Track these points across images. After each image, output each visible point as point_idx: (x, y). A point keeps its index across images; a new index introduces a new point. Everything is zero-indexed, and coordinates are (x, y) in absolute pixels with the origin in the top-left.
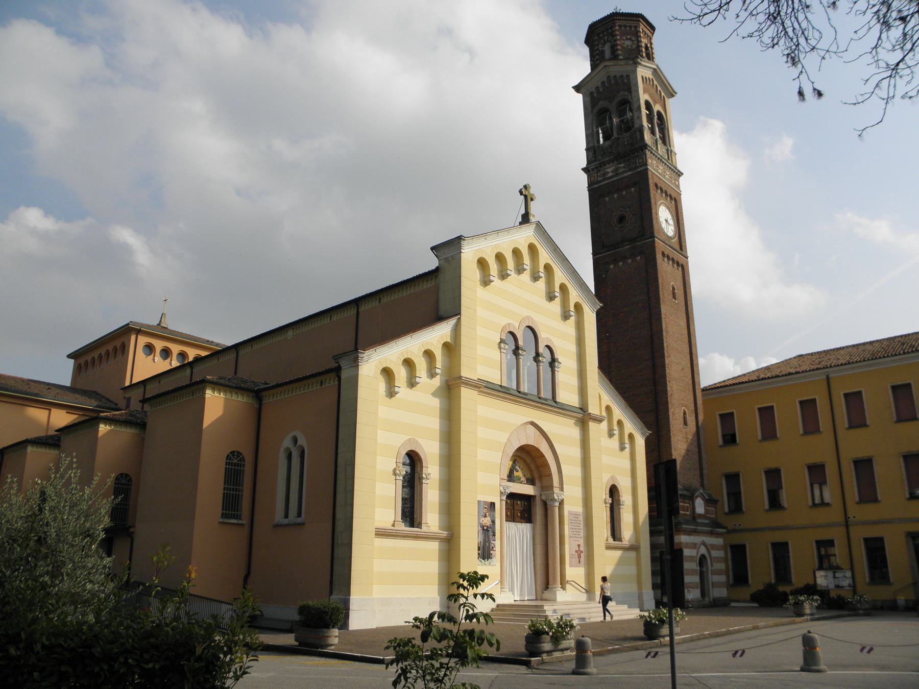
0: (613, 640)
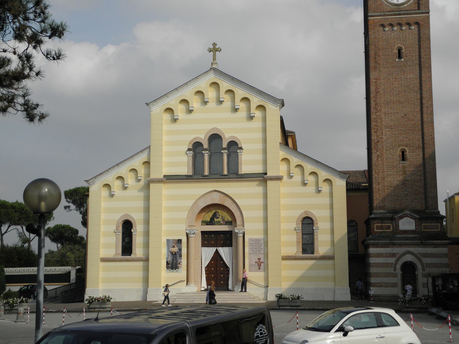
0: (308, 259)
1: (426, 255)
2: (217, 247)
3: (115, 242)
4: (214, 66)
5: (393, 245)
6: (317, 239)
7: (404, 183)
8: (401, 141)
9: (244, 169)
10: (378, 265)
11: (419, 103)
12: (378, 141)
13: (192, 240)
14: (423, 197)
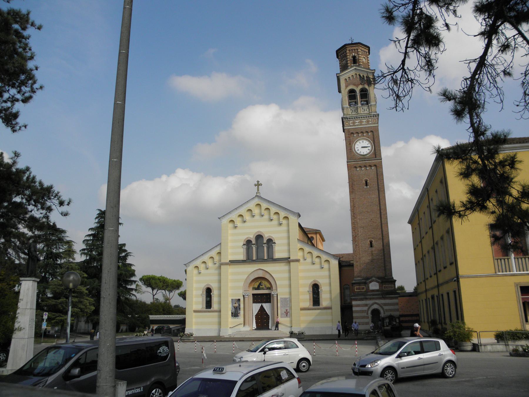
1: (385, 304)
2: (262, 303)
3: (201, 300)
4: (258, 195)
5: (366, 299)
6: (322, 297)
7: (372, 261)
8: (369, 235)
9: (277, 255)
10: (357, 312)
11: (379, 212)
12: (356, 236)
13: (246, 299)
14: (384, 269)
